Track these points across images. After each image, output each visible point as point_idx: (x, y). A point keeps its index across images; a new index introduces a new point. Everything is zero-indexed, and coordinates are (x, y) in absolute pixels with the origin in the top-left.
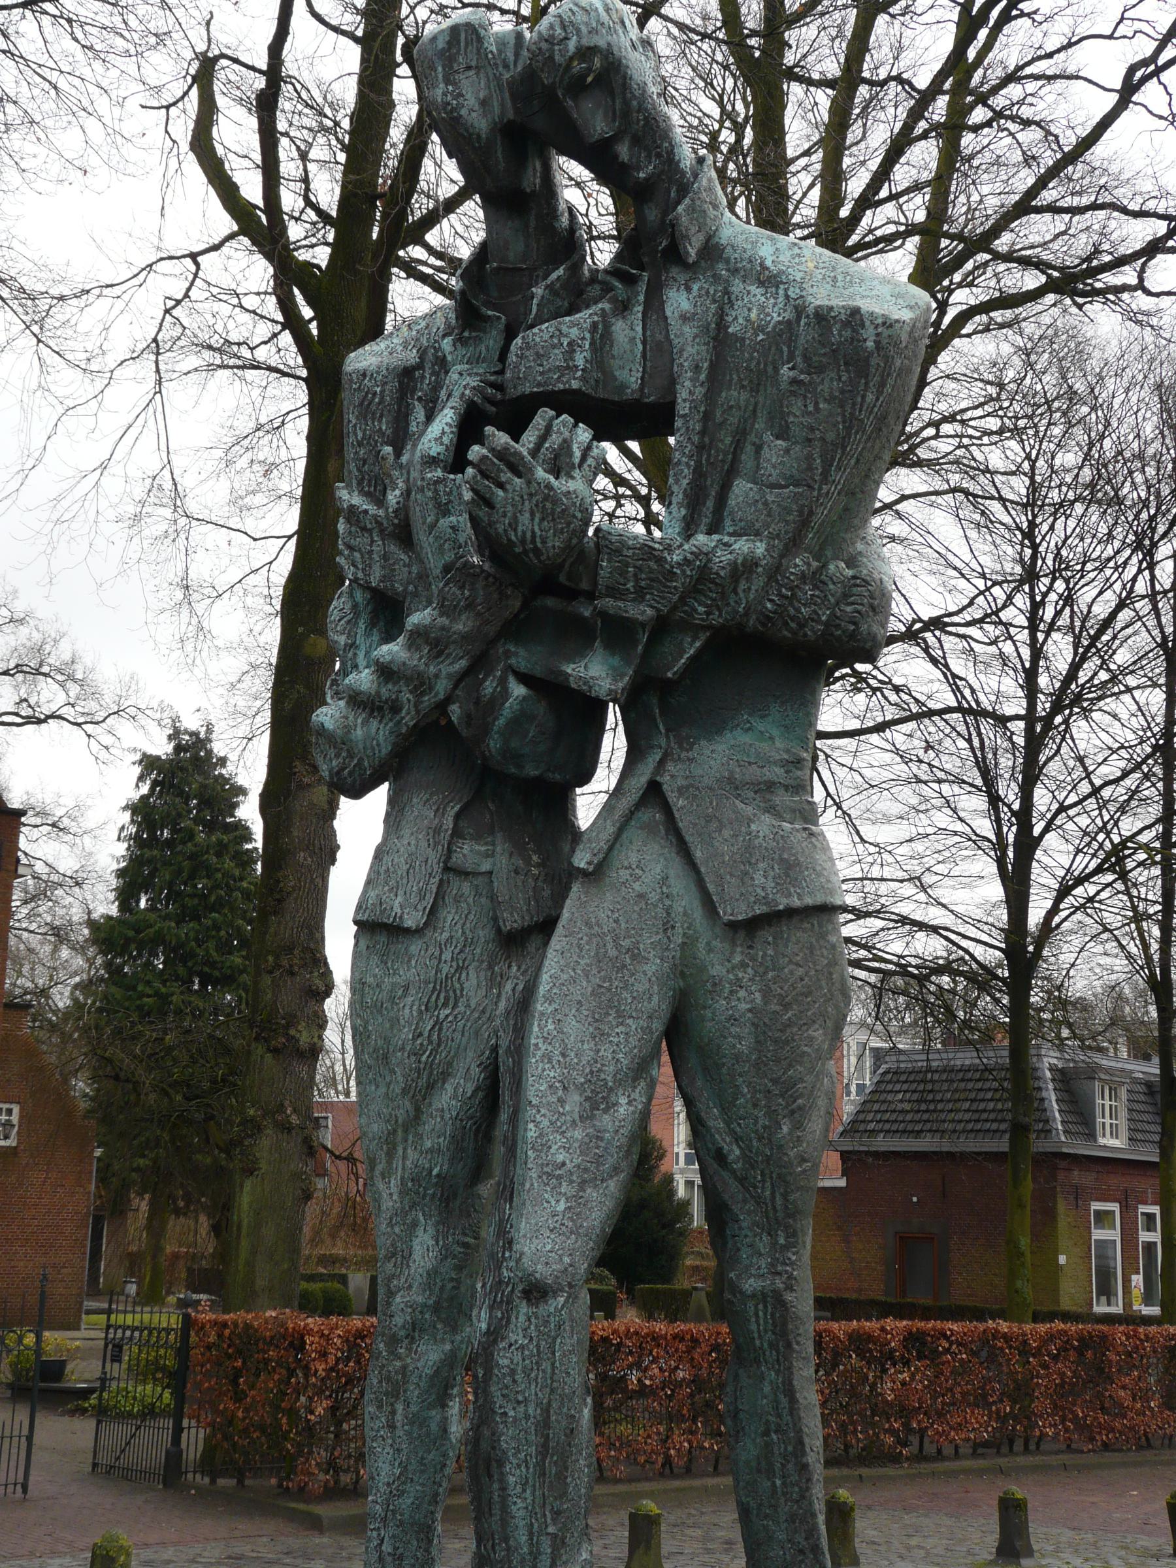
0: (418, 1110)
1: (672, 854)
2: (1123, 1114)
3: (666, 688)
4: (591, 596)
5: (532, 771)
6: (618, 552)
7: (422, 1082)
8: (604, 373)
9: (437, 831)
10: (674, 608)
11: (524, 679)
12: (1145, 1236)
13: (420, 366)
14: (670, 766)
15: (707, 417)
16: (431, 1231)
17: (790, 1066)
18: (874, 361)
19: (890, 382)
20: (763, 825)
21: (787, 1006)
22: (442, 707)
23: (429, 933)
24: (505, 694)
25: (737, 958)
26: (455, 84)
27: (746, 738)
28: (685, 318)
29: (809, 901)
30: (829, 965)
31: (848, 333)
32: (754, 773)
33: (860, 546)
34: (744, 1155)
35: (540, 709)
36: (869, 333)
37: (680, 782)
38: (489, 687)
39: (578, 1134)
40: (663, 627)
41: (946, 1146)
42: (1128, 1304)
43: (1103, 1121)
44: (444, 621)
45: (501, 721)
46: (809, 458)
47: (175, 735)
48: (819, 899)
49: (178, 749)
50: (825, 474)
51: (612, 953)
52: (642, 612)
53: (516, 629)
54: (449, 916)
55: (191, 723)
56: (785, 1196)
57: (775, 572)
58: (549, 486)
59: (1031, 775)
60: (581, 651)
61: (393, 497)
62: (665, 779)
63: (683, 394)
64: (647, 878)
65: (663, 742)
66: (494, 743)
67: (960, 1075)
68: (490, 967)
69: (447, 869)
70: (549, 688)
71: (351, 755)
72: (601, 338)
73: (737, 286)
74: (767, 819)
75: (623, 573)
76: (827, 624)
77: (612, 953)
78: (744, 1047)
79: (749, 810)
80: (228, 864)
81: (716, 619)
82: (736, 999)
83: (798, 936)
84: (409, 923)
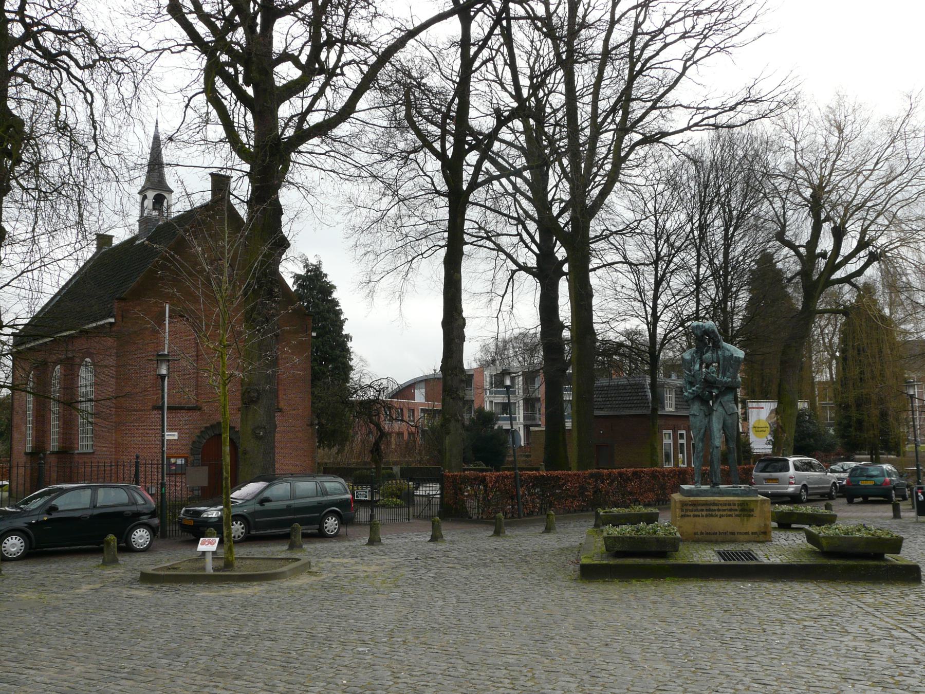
2: (674, 399)
12: (680, 441)
41: (616, 414)
42: (676, 464)
43: (667, 402)
47: (306, 266)
49: (308, 271)
55: (313, 261)
59: (656, 298)
80: (332, 316)
82: (729, 421)
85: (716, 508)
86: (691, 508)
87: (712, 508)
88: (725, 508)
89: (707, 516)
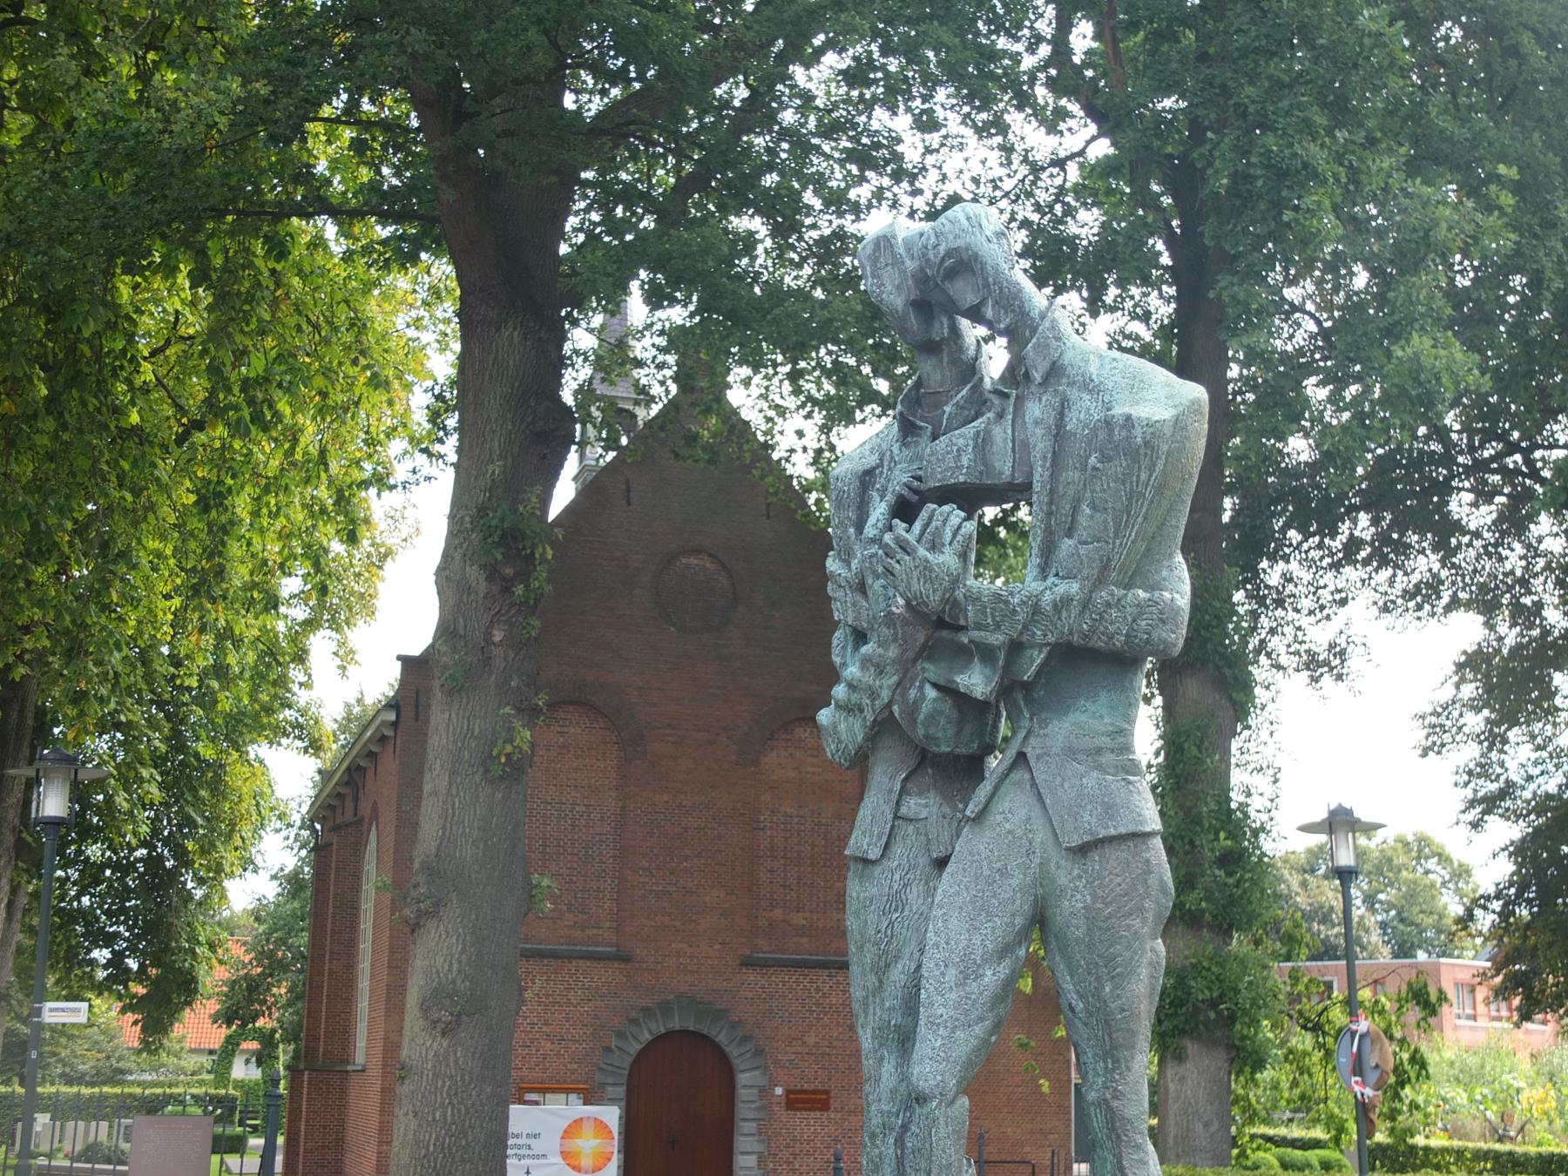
0: (880, 981)
1: (1033, 800)
3: (1027, 687)
4: (964, 628)
5: (945, 749)
6: (978, 599)
7: (882, 964)
8: (985, 464)
9: (890, 791)
10: (1021, 633)
11: (935, 685)
13: (881, 465)
14: (1033, 741)
15: (1052, 491)
16: (893, 1063)
17: (1111, 946)
18: (1142, 451)
19: (1160, 465)
20: (1091, 780)
21: (1107, 905)
22: (889, 704)
23: (885, 862)
24: (923, 697)
25: (1076, 872)
26: (878, 277)
27: (1083, 718)
28: (1036, 423)
29: (1123, 830)
30: (1144, 873)
31: (1124, 433)
32: (1087, 743)
33: (1164, 573)
34: (1086, 1008)
35: (947, 706)
36: (1138, 432)
37: (1038, 751)
38: (913, 693)
39: (953, 996)
40: (1016, 648)
44: (880, 650)
45: (922, 717)
46: (1105, 521)
48: (1131, 828)
50: (1116, 535)
51: (986, 872)
52: (996, 639)
53: (928, 652)
54: (898, 849)
56: (1110, 1035)
57: (1086, 604)
58: (927, 561)
60: (966, 666)
61: (854, 564)
62: (1028, 751)
63: (1036, 477)
64: (1016, 819)
65: (1027, 723)
66: (921, 731)
68: (927, 883)
69: (896, 817)
70: (948, 690)
71: (840, 742)
72: (983, 443)
73: (1073, 394)
74: (1095, 774)
75: (984, 613)
76: (1127, 636)
77: (986, 872)
78: (1079, 934)
79: (1082, 769)
81: (1051, 639)
83: (1115, 857)
84: (872, 856)
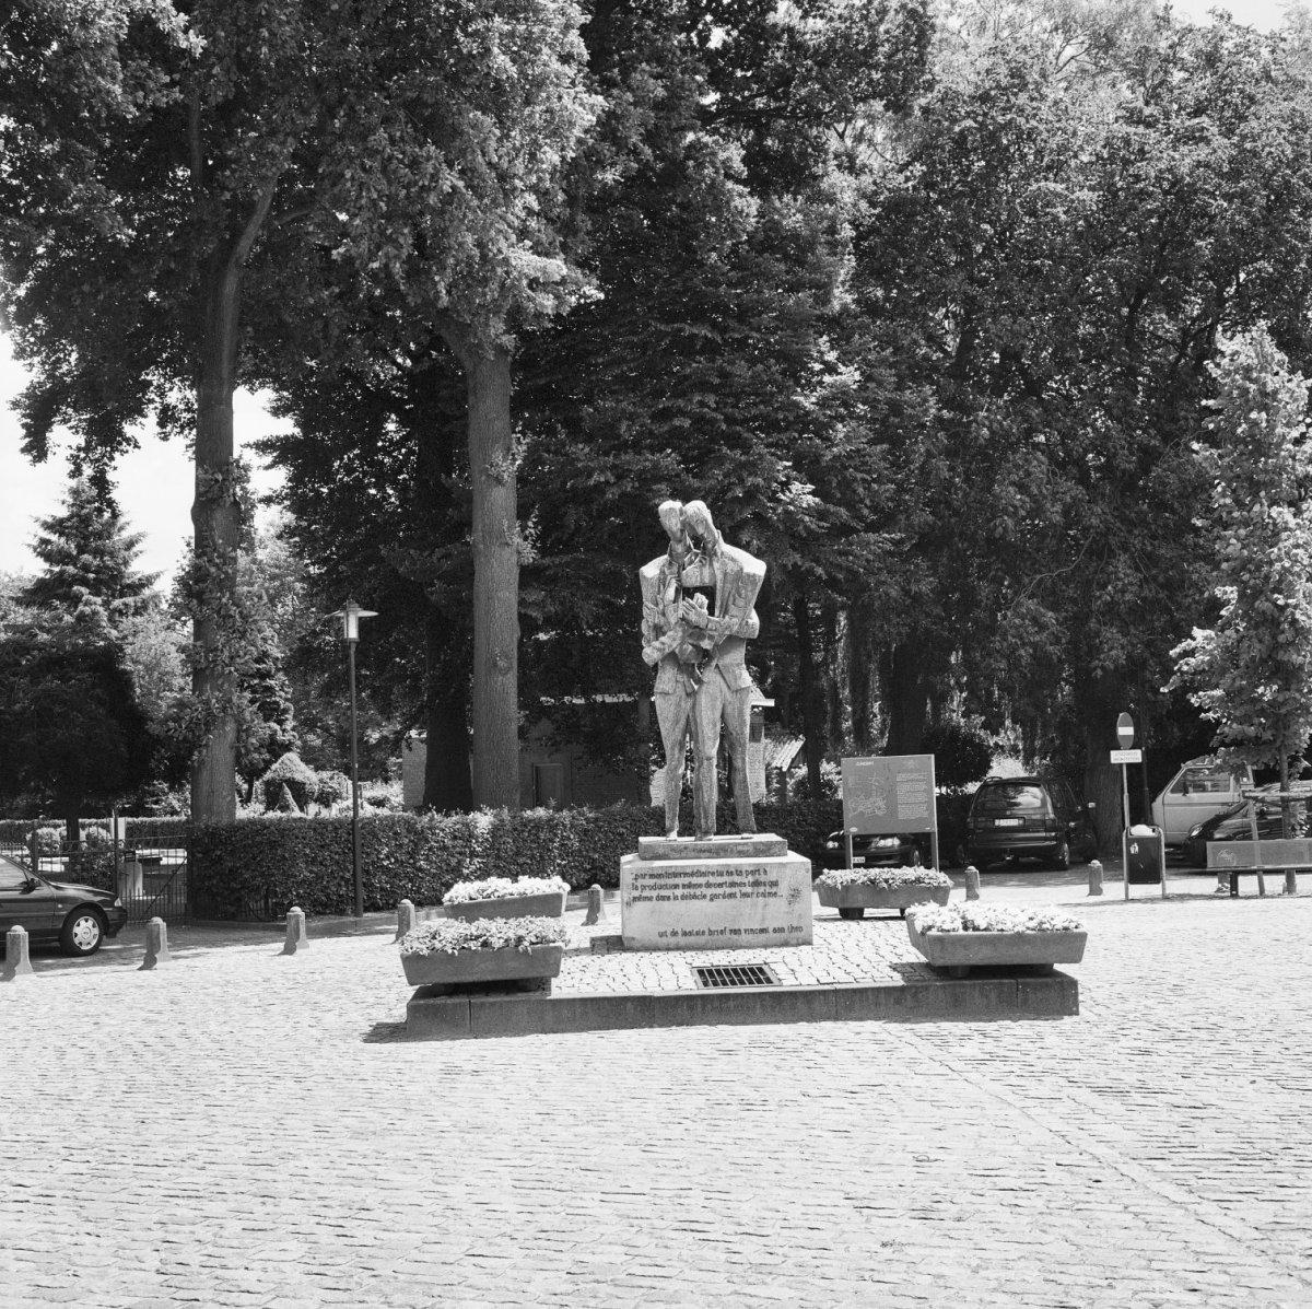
67: (751, 879)
85: (702, 880)
86: (652, 882)
87: (695, 880)
88: (720, 880)
89: (684, 897)
